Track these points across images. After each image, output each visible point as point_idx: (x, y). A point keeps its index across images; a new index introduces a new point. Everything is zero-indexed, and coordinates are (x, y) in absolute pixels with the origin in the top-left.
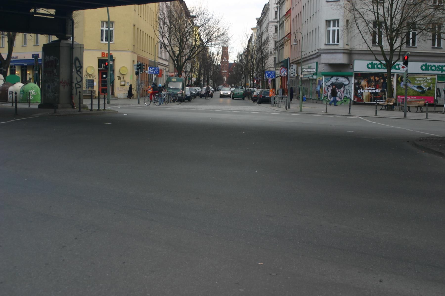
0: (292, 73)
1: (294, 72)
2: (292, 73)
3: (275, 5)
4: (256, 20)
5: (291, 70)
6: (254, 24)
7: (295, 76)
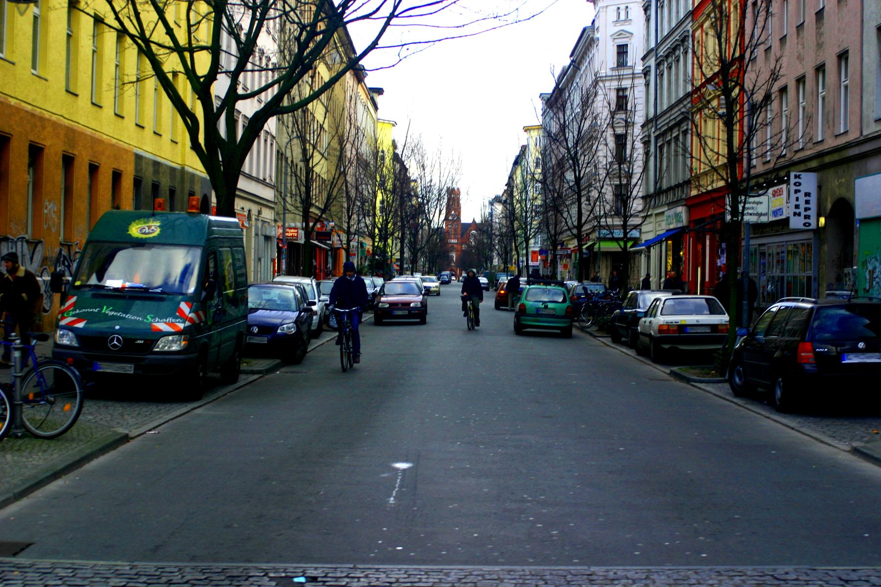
0: (795, 214)
1: (806, 209)
2: (795, 214)
3: (615, 26)
4: (540, 99)
5: (793, 196)
6: (534, 113)
7: (810, 224)
